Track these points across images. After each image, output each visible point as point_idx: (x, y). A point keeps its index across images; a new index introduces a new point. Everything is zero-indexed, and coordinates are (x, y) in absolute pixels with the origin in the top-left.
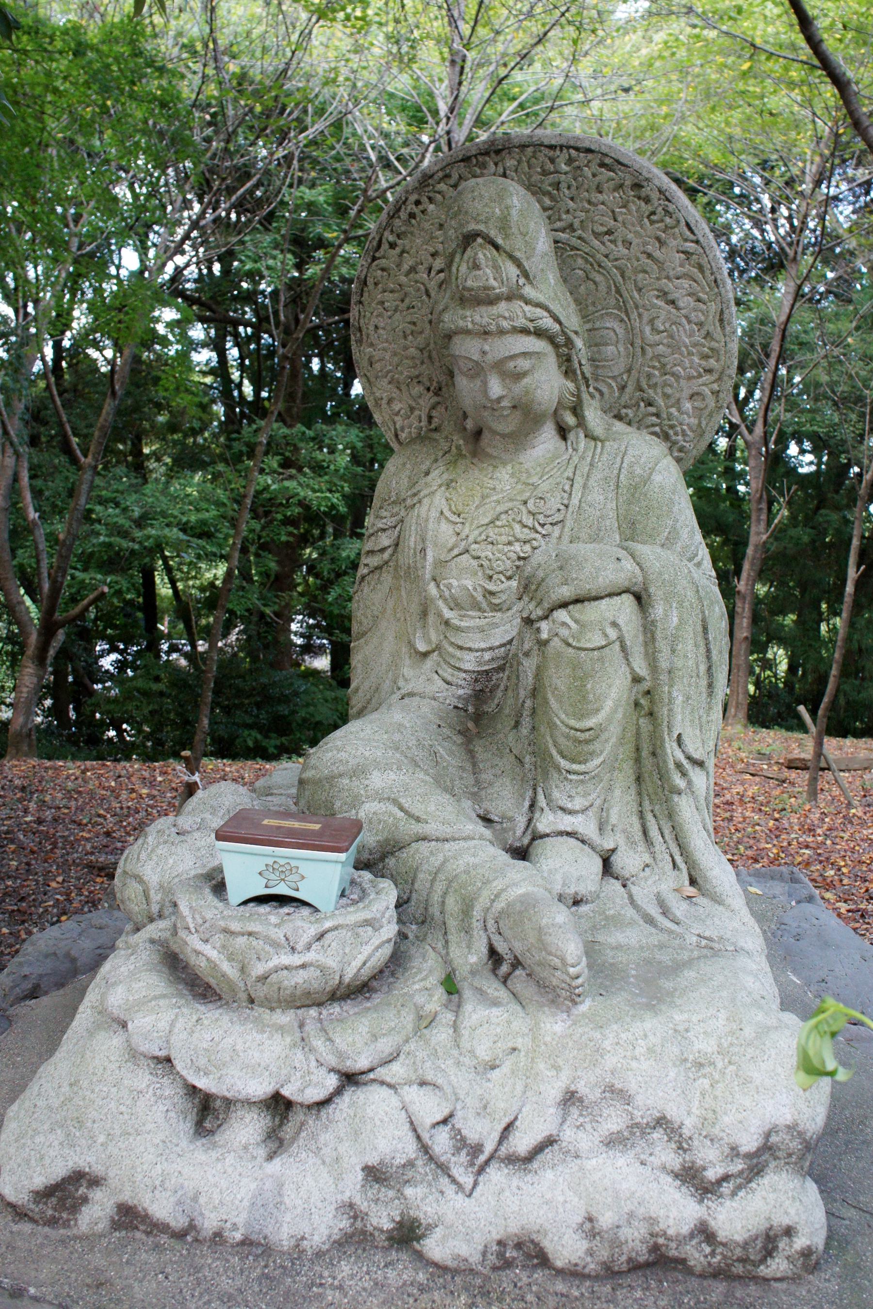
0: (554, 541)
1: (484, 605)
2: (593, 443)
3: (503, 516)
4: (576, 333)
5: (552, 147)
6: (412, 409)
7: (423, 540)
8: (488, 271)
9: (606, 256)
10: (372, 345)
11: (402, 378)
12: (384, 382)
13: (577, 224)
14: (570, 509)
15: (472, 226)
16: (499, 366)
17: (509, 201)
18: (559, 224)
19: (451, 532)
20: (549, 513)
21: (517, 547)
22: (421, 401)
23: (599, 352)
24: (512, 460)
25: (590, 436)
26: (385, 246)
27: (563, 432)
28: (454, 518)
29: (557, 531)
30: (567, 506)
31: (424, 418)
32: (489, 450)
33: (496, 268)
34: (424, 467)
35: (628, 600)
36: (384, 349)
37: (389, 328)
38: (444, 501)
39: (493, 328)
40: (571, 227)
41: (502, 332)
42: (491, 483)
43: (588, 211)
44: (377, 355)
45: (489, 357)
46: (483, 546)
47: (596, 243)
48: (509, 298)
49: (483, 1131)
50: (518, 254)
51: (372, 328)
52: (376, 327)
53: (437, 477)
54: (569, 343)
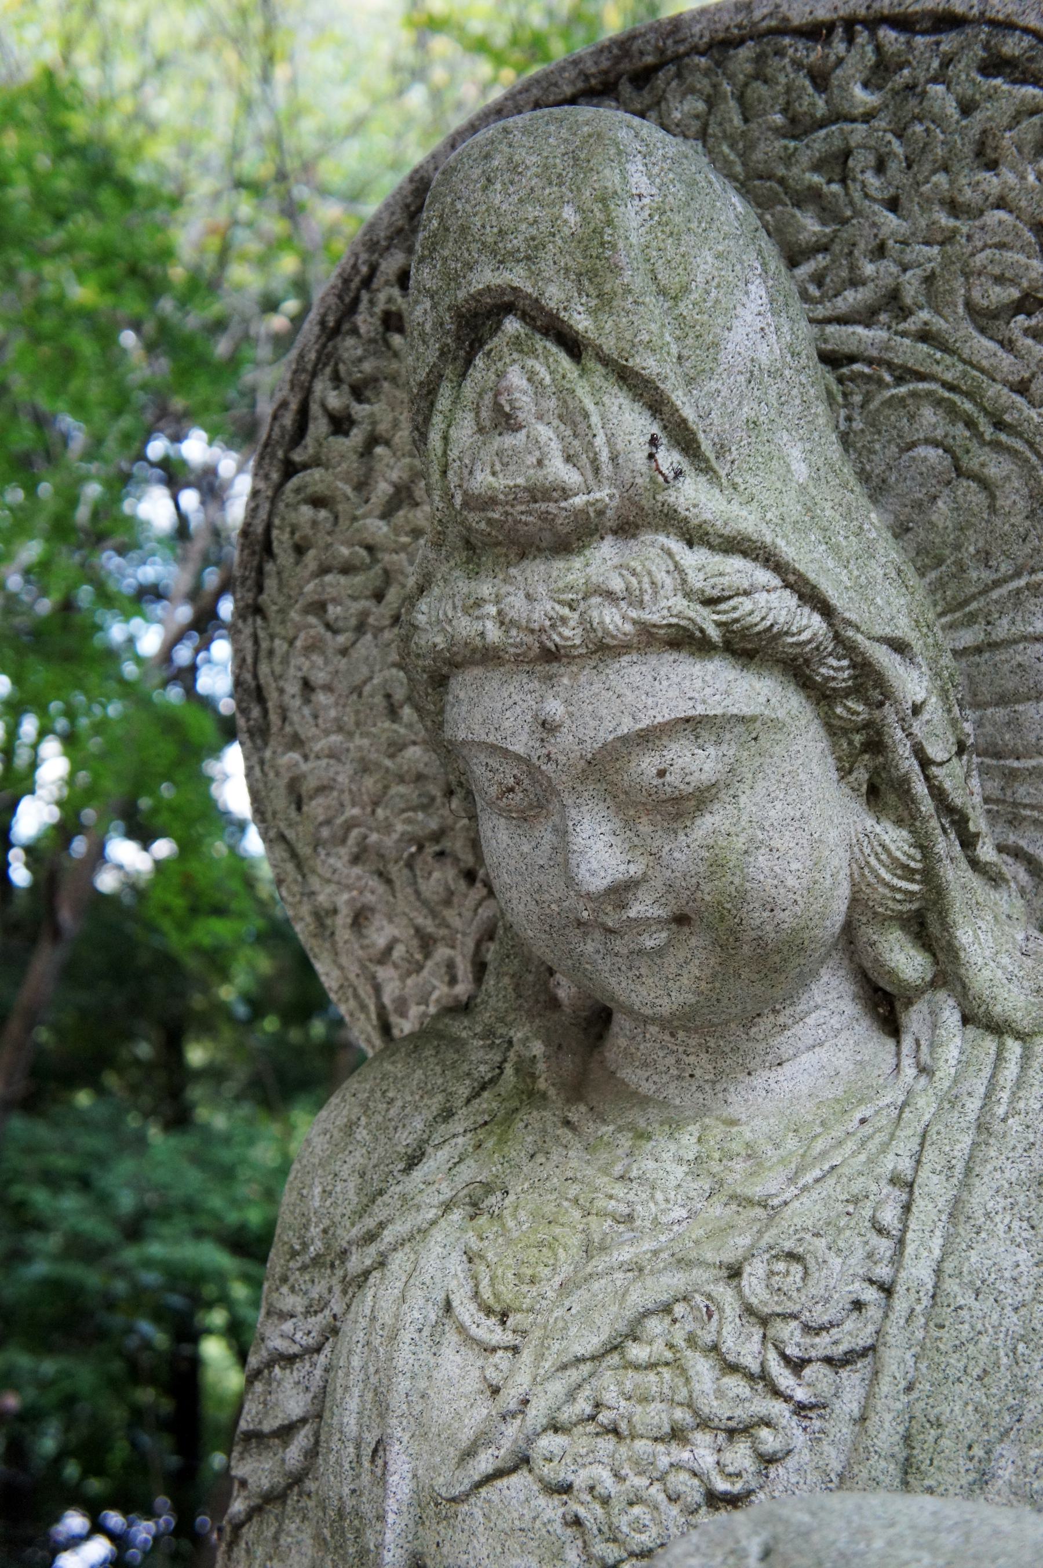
0: (842, 1430)
2: (990, 1044)
3: (655, 1326)
4: (899, 647)
5: (816, 32)
6: (426, 943)
7: (382, 1409)
8: (544, 432)
9: (1022, 388)
10: (296, 742)
11: (389, 841)
12: (338, 860)
13: (912, 289)
14: (900, 1305)
15: (486, 277)
16: (603, 769)
17: (611, 177)
18: (852, 298)
19: (472, 1384)
20: (820, 1315)
21: (703, 1451)
22: (450, 915)
23: (1013, 724)
24: (704, 1110)
25: (977, 1018)
26: (319, 426)
27: (885, 1006)
28: (489, 1331)
30: (887, 1290)
31: (464, 968)
32: (632, 1076)
33: (573, 418)
34: (405, 1139)
36: (333, 755)
37: (342, 687)
38: (456, 1263)
39: (571, 634)
40: (893, 302)
41: (603, 649)
42: (618, 1197)
43: (949, 238)
44: (314, 772)
45: (565, 739)
46: (581, 1441)
47: (982, 347)
48: (626, 528)
50: (648, 364)
51: (293, 688)
52: (307, 686)
53: (437, 1177)
54: (868, 681)
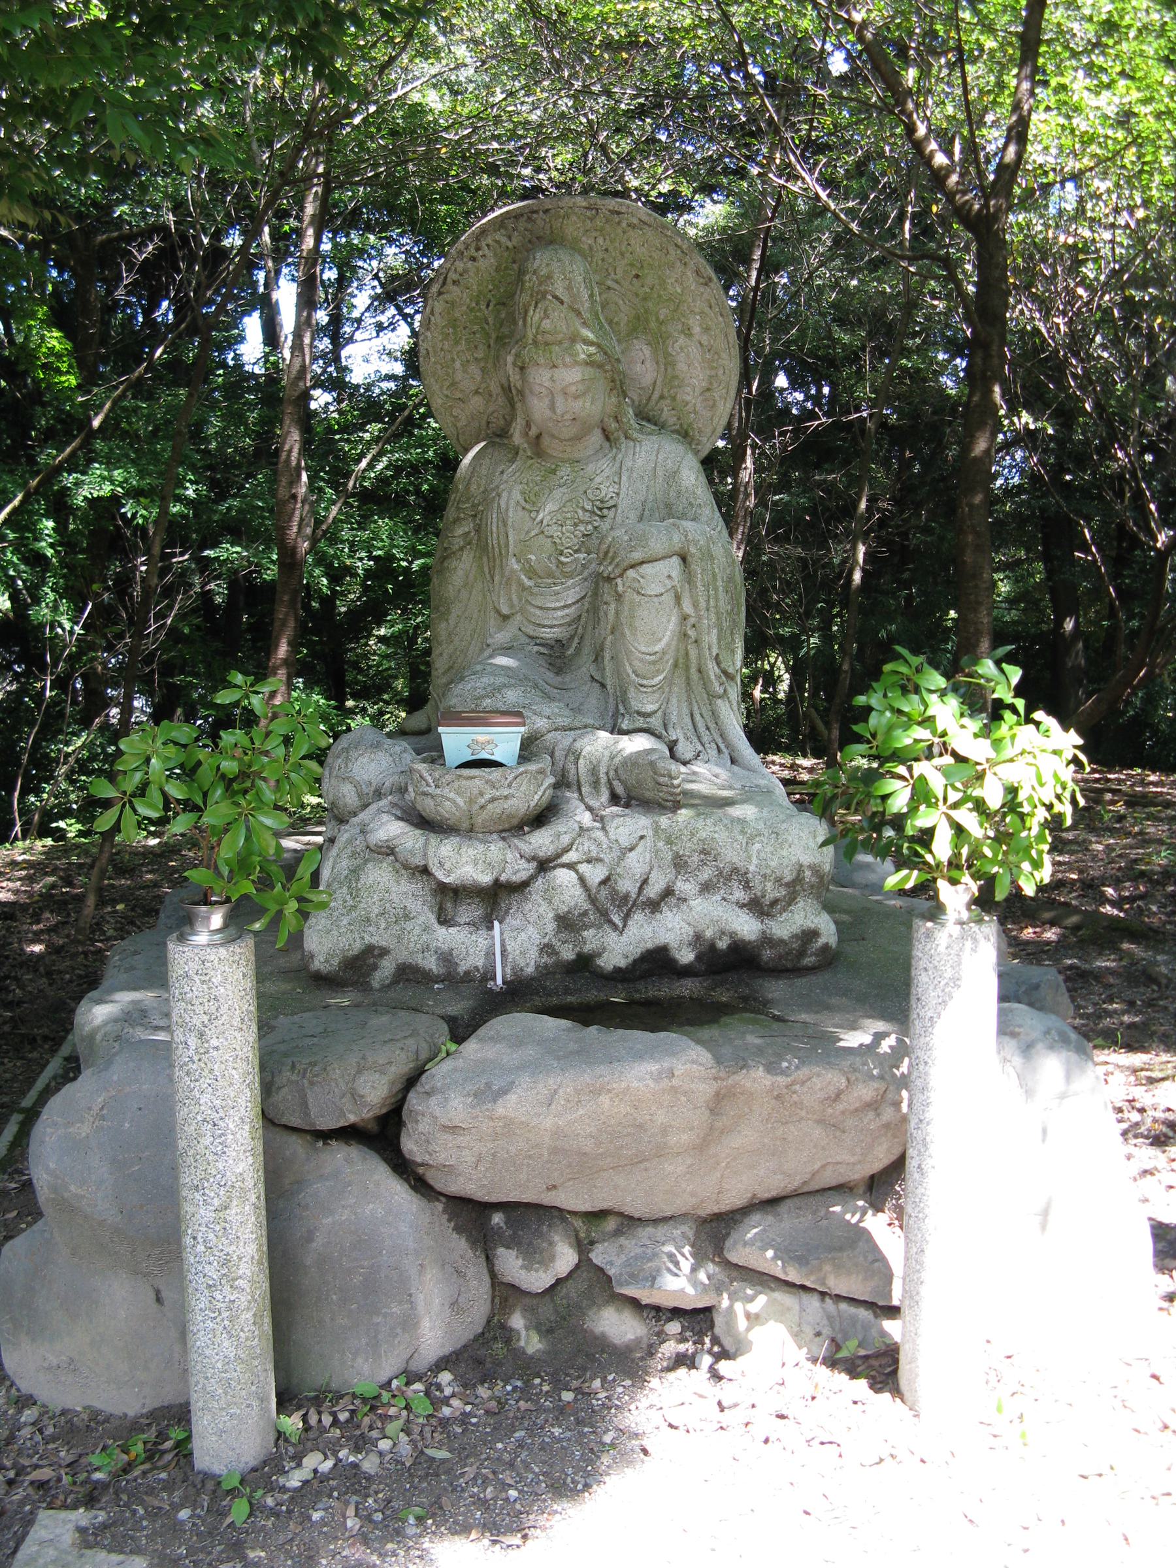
1: (557, 574)
29: (611, 514)
35: (675, 560)
49: (627, 886)
